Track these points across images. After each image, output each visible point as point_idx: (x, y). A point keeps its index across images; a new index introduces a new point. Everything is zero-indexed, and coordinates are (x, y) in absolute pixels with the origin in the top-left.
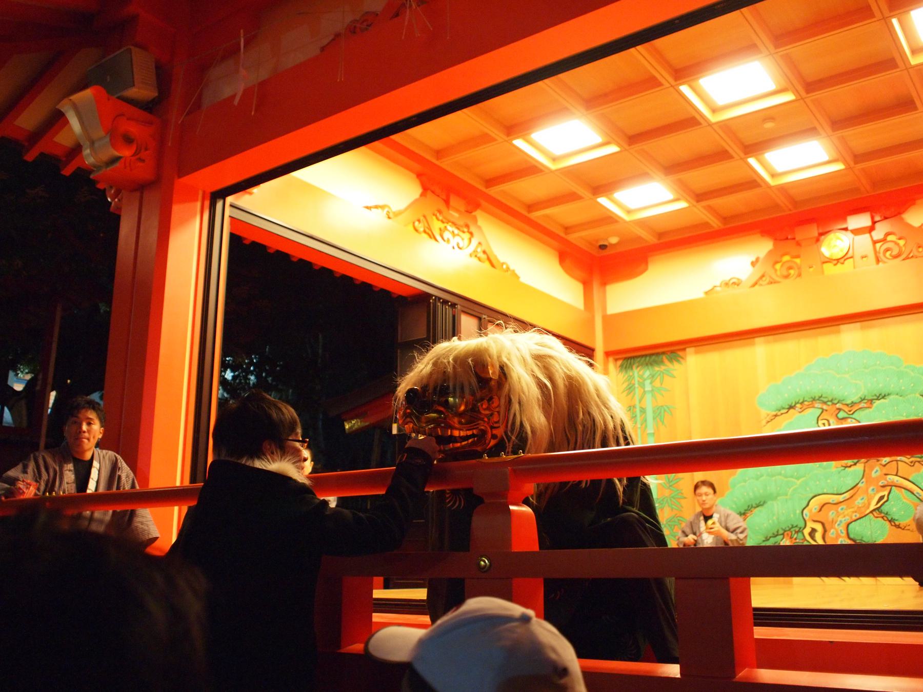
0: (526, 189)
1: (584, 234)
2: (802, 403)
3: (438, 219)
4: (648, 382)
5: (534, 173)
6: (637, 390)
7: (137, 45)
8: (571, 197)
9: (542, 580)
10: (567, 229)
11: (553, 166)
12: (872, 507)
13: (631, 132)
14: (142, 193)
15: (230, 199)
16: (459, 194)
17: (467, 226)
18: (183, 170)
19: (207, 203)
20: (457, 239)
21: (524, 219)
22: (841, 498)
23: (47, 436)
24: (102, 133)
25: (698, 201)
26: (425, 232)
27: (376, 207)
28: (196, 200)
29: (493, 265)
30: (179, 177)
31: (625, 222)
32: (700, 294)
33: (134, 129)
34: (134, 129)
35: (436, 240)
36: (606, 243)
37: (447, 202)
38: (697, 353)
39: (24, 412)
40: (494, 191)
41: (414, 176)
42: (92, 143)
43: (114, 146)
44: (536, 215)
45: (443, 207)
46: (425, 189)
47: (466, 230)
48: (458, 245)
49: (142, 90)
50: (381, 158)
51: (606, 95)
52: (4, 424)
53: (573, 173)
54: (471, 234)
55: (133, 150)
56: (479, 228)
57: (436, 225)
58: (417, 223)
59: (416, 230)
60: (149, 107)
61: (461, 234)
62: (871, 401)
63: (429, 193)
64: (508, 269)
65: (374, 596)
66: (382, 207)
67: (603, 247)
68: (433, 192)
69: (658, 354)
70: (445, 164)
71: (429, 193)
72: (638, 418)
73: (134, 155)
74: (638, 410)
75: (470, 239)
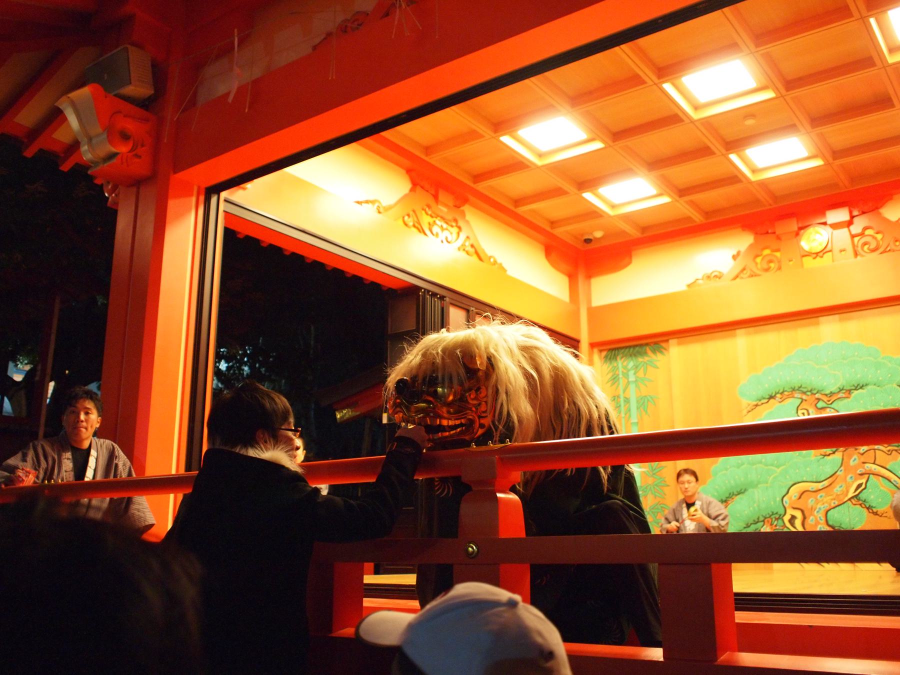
0: (512, 185)
1: (569, 228)
2: (782, 393)
3: (427, 214)
4: (631, 373)
5: (520, 169)
6: (621, 380)
7: (134, 44)
8: (557, 192)
9: (528, 565)
10: (553, 223)
11: (539, 162)
12: (851, 495)
13: (615, 129)
14: (138, 188)
15: (224, 195)
16: (447, 189)
17: (456, 220)
18: (179, 166)
19: (202, 198)
20: (446, 233)
21: (511, 214)
22: (820, 486)
23: (46, 425)
24: (99, 130)
25: (680, 196)
26: (414, 226)
27: (367, 202)
28: (192, 195)
29: (480, 259)
30: (175, 173)
31: (609, 216)
32: (682, 287)
33: (130, 126)
34: (130, 126)
35: (425, 234)
36: (591, 237)
37: (436, 197)
38: (679, 344)
39: (24, 402)
40: (482, 187)
41: (404, 172)
42: (90, 139)
43: (111, 142)
44: (522, 210)
45: (432, 202)
46: (415, 184)
47: (454, 224)
48: (447, 239)
49: (139, 88)
50: (371, 154)
51: (591, 93)
52: (4, 414)
53: (558, 168)
54: (460, 228)
55: (130, 146)
56: (468, 222)
57: (426, 220)
58: (406, 218)
59: (406, 225)
60: (145, 104)
61: (449, 228)
62: (849, 392)
63: (418, 189)
64: (495, 263)
65: (365, 582)
66: (373, 202)
67: (588, 241)
68: (422, 187)
69: (641, 345)
70: (434, 160)
71: (418, 189)
72: (622, 408)
73: (131, 151)
74: (622, 400)
75: (458, 233)
